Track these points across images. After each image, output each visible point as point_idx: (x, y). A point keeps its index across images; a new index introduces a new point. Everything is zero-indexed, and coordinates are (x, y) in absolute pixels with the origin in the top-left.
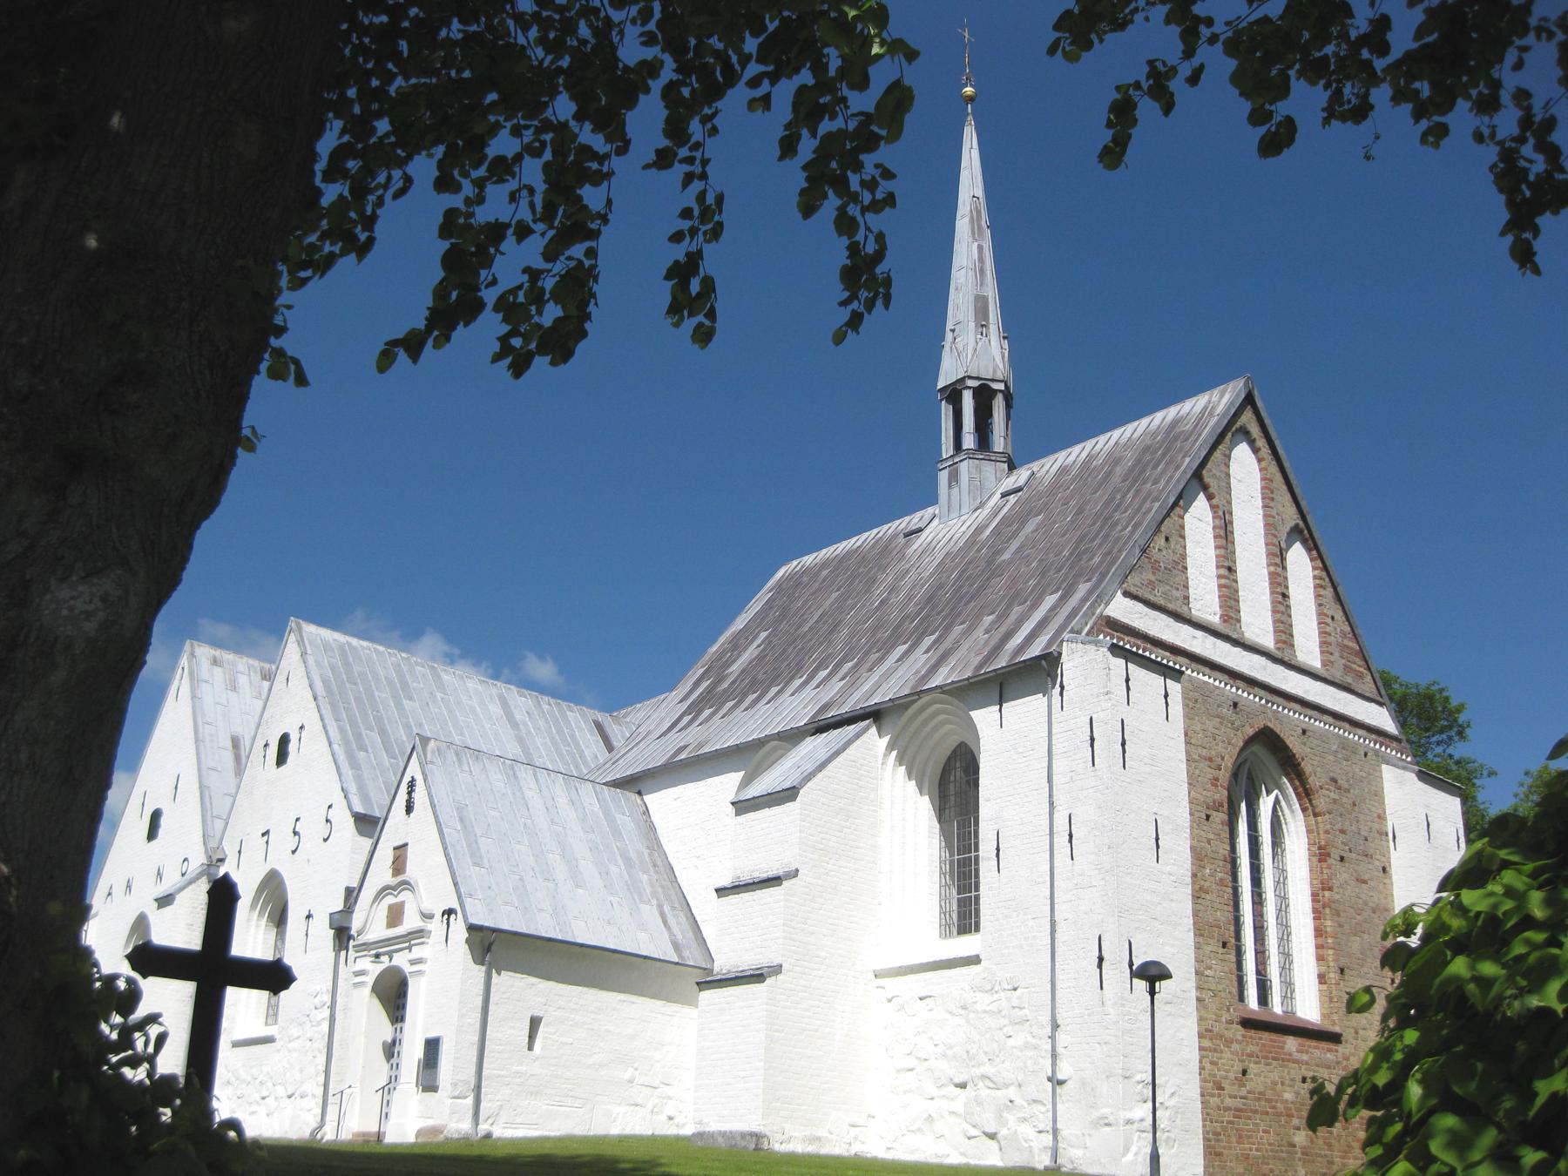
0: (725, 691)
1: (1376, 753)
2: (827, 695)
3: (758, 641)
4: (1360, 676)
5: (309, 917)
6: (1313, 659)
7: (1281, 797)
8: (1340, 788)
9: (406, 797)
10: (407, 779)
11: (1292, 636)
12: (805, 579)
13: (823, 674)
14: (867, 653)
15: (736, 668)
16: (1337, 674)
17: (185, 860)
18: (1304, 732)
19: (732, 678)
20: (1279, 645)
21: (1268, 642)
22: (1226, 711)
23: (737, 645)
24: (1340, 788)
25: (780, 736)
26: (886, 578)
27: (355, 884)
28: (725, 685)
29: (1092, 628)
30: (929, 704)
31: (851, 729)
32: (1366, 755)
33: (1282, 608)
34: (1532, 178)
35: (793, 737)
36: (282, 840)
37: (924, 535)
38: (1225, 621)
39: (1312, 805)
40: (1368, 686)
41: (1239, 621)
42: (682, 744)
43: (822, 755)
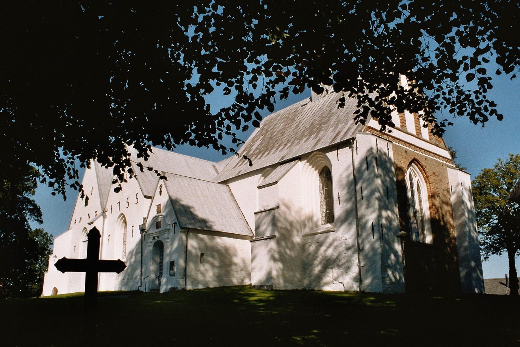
0: (251, 154)
1: (446, 165)
2: (283, 154)
3: (260, 139)
4: (440, 142)
5: (133, 226)
6: (427, 138)
7: (419, 179)
8: (436, 175)
9: (160, 190)
10: (159, 185)
11: (421, 131)
12: (272, 120)
13: (266, 153)
14: (294, 140)
15: (254, 147)
16: (434, 142)
17: (96, 211)
18: (425, 159)
19: (253, 150)
20: (417, 134)
21: (414, 133)
22: (404, 154)
23: (253, 141)
24: (436, 175)
25: (270, 166)
26: (297, 120)
27: (146, 216)
28: (251, 152)
29: (365, 130)
30: (315, 155)
31: (292, 163)
32: (443, 165)
33: (418, 122)
34: (483, 37)
35: (274, 166)
36: (124, 204)
37: (307, 106)
38: (402, 127)
39: (428, 181)
40: (442, 145)
41: (406, 127)
42: (240, 170)
43: (284, 172)
